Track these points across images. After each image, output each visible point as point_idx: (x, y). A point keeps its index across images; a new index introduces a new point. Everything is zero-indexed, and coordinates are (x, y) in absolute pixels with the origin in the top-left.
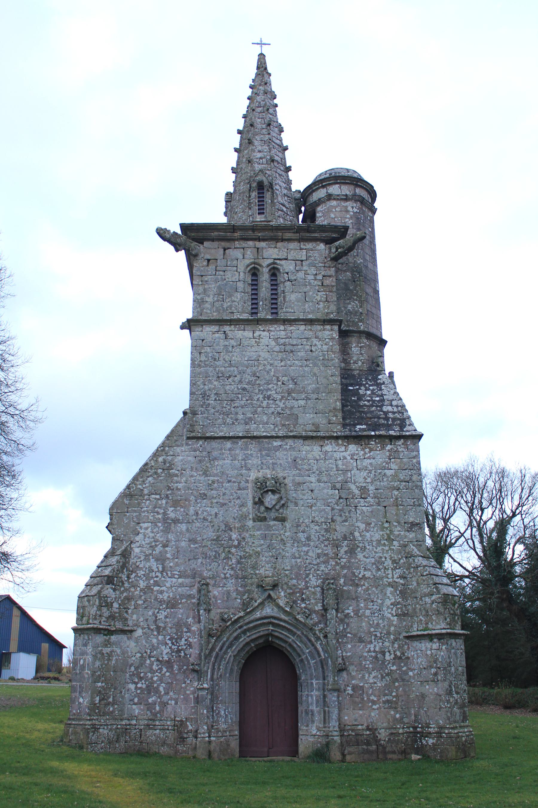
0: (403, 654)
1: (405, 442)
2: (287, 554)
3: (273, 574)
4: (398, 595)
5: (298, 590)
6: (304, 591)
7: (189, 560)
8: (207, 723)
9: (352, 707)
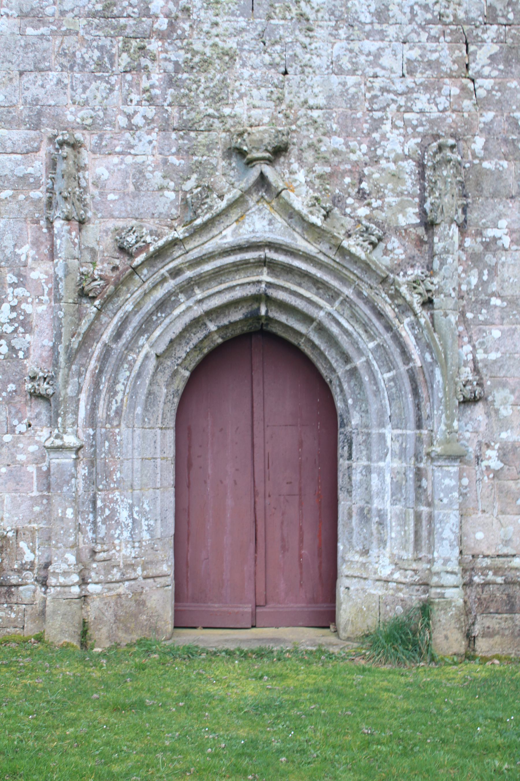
2: (316, 61)
3: (273, 118)
5: (348, 167)
6: (366, 171)
7: (21, 73)
8: (75, 545)
9: (497, 505)
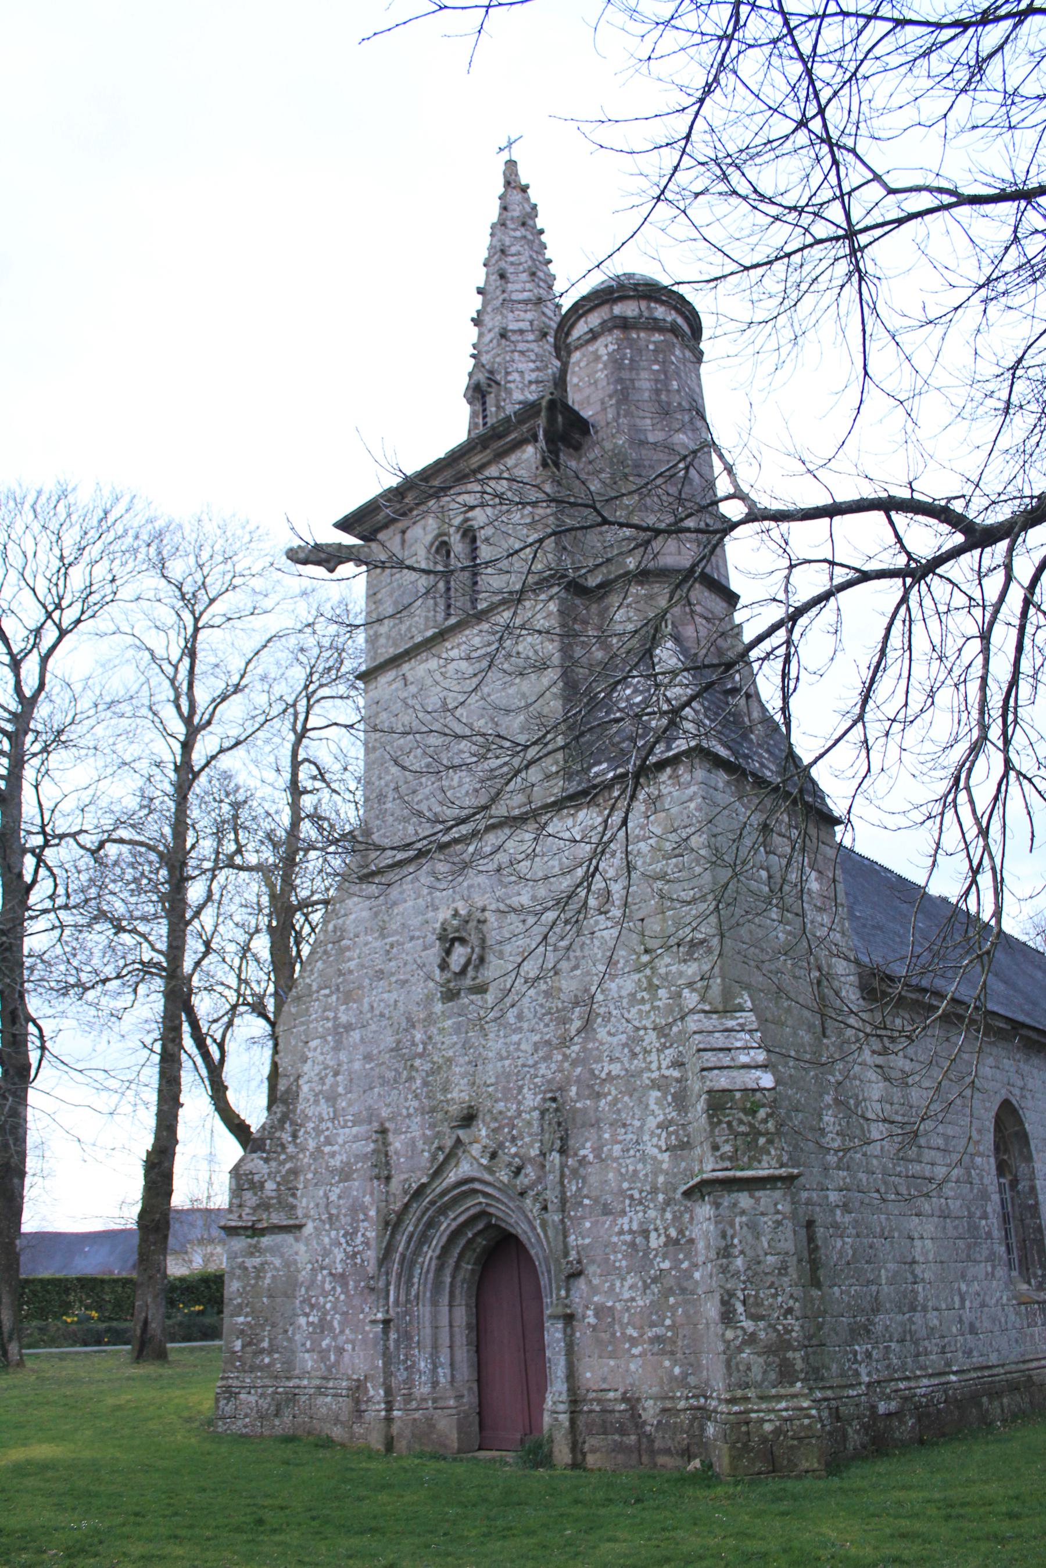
0: (681, 1232)
1: (674, 770)
4: (669, 1105)
